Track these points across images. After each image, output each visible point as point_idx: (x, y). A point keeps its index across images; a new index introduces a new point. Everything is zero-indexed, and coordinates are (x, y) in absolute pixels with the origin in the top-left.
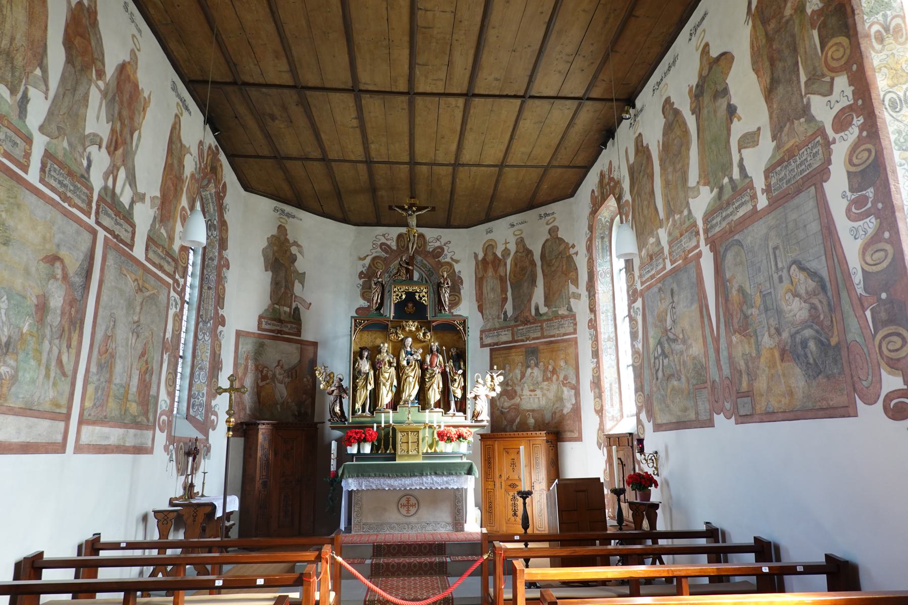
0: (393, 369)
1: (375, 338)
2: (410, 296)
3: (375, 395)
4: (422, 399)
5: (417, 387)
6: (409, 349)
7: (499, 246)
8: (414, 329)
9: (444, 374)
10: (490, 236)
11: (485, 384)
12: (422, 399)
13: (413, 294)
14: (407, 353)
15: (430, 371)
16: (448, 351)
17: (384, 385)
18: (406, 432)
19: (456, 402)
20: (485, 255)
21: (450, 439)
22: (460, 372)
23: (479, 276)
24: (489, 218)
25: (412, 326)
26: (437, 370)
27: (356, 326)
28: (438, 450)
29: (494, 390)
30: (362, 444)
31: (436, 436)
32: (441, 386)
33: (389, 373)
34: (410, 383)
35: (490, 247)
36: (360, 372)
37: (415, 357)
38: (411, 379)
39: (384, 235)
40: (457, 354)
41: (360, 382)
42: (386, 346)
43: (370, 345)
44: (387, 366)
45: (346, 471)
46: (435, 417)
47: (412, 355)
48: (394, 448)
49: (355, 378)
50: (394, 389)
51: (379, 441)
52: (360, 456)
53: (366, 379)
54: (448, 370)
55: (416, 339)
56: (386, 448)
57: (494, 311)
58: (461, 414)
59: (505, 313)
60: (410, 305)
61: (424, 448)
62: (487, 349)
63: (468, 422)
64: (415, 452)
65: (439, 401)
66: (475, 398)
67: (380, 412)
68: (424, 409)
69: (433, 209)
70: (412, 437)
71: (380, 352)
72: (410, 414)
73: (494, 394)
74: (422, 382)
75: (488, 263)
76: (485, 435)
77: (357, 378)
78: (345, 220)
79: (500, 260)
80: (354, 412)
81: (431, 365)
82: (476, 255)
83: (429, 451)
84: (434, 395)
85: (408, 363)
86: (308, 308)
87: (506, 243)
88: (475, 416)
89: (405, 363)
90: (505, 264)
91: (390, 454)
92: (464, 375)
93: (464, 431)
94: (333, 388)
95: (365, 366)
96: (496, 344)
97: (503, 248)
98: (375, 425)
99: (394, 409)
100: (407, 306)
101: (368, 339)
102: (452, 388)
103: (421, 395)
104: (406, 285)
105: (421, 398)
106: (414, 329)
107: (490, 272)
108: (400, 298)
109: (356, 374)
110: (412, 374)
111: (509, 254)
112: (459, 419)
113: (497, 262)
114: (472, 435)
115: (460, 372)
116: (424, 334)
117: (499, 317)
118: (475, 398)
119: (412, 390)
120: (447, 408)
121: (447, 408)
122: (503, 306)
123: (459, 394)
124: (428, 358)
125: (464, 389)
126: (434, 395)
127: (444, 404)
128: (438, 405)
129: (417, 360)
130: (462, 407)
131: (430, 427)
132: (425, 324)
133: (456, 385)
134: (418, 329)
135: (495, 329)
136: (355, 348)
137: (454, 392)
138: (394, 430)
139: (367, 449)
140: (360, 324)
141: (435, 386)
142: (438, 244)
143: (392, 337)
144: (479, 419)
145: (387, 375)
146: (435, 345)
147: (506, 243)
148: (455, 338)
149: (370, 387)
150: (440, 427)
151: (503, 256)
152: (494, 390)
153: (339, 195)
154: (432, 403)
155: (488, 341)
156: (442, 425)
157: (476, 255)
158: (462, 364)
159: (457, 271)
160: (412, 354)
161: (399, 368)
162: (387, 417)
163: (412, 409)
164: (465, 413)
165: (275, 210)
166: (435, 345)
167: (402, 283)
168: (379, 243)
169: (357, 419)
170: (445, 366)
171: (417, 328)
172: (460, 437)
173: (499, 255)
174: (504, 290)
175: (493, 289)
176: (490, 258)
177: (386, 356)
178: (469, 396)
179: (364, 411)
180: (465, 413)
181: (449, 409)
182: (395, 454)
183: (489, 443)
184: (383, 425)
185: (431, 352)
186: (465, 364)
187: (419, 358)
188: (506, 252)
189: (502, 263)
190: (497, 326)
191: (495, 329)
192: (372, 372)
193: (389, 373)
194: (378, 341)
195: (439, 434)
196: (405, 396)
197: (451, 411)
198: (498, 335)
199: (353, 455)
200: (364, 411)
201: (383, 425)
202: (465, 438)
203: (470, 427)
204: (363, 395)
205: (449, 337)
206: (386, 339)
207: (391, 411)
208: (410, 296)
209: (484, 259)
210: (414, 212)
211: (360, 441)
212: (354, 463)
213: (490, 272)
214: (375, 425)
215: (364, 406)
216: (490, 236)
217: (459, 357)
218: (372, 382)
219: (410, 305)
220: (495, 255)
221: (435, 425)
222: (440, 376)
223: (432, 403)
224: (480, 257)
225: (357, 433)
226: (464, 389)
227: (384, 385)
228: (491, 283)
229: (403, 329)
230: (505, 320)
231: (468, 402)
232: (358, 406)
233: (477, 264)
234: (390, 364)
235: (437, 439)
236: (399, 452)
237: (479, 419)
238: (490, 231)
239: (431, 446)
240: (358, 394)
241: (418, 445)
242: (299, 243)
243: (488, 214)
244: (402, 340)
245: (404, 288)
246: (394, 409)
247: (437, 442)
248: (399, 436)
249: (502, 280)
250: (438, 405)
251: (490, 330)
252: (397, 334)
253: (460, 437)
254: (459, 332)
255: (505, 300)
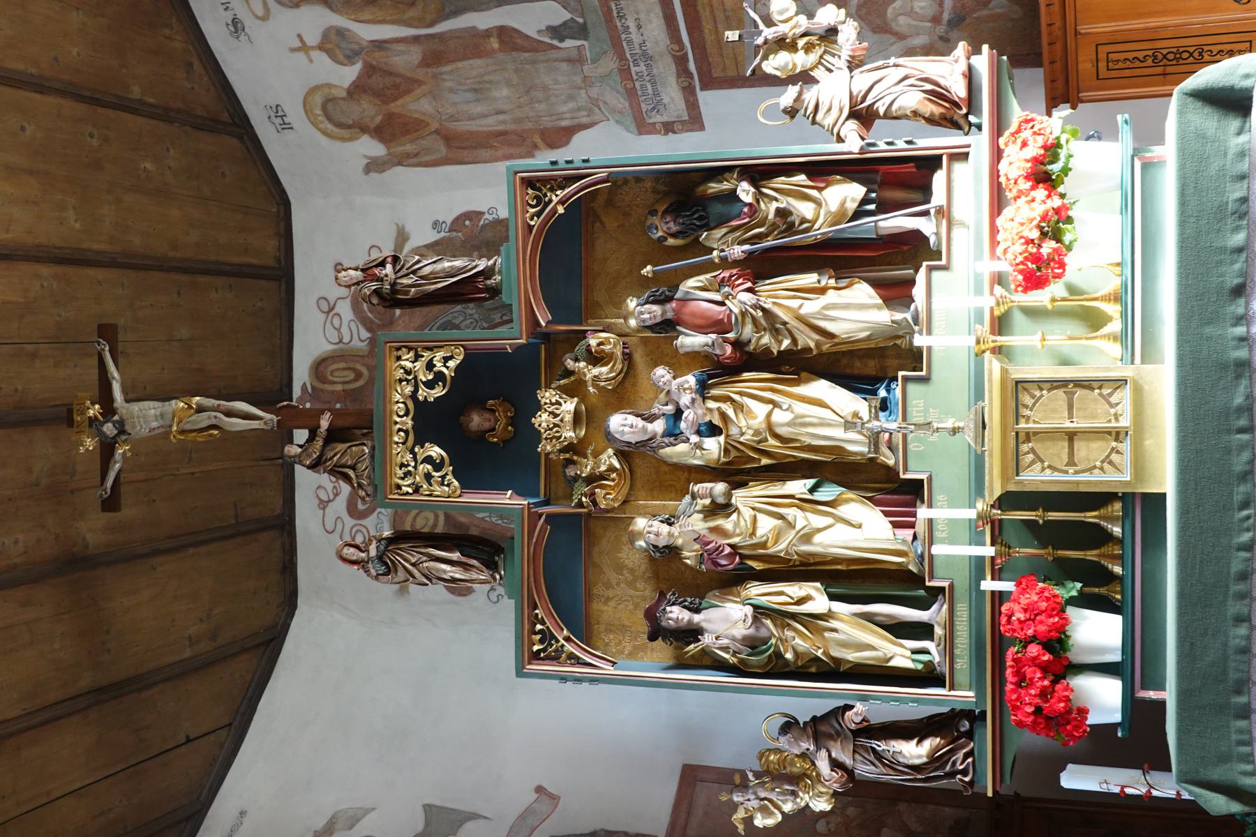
0: (740, 497)
1: (619, 568)
2: (431, 422)
3: (854, 579)
4: (871, 367)
5: (821, 388)
6: (659, 426)
7: (322, 79)
8: (569, 406)
9: (762, 266)
10: (295, 114)
11: (805, 78)
12: (871, 367)
13: (422, 411)
14: (673, 434)
15: (748, 331)
16: (660, 252)
17: (807, 538)
18: (1019, 441)
19: (886, 207)
20: (364, 130)
21: (1054, 226)
22: (745, 192)
23: (443, 150)
24: (231, 121)
25: (556, 413)
26: (743, 298)
27: (555, 658)
28: (1112, 284)
29: (832, 32)
30: (1075, 657)
31: (1039, 298)
32: (810, 279)
33: (757, 517)
34: (797, 422)
35: (333, 114)
36: (754, 644)
37: (685, 400)
38: (779, 417)
39: (323, 505)
40: (675, 210)
41: (797, 643)
42: (649, 528)
43: (647, 594)
44: (728, 524)
45: (1217, 774)
46: (952, 306)
47: (678, 414)
48: (1099, 499)
49: (778, 668)
50: (828, 492)
51: (1065, 571)
52: (1133, 667)
53: (782, 617)
54: (738, 251)
55: (622, 395)
56: (1099, 537)
57: (557, 79)
58: (939, 179)
59: (558, 32)
60: (477, 421)
61: (1101, 356)
62: (709, 100)
63: (979, 144)
64: (1124, 397)
65: (876, 284)
66: (863, 115)
67: (926, 559)
68: (915, 358)
69: (107, 332)
70: (1047, 414)
71: (671, 552)
72: (938, 423)
73: (849, 33)
74: (796, 365)
75: (390, 117)
76: (1050, 83)
77: (778, 655)
78: (267, 645)
79: (369, 70)
80: (928, 677)
81: (719, 326)
82: (374, 166)
83: (1115, 326)
84: (852, 310)
85: (713, 430)
86: (554, 798)
87: (304, 48)
88: (951, 113)
89: (713, 445)
90: (379, 45)
91: (1127, 515)
92: (760, 174)
93: (1016, 163)
94: (823, 765)
95: (726, 621)
96: (681, 61)
97: (321, 58)
98: (988, 585)
99: (914, 491)
100: (481, 435)
101: (621, 601)
102: (822, 229)
103: (858, 367)
104: (385, 444)
105: (871, 368)
106: (569, 406)
107: (419, 105)
108: (438, 466)
109: (762, 662)
110: (760, 410)
111: (341, 33)
112: (962, 188)
113: (377, 81)
114: (1037, 124)
115: (745, 192)
116: (596, 359)
117: (577, 60)
118: (863, 115)
119: (827, 412)
120: (912, 249)
121: (912, 249)
122: (532, 46)
123: (845, 194)
124: (691, 341)
125: (823, 171)
126: (852, 310)
127: (893, 262)
128: (896, 293)
129: (703, 389)
130: (906, 179)
131: (1001, 324)
132: (546, 357)
133: (805, 209)
134: (575, 388)
135: (625, 72)
136: (652, 663)
137: (839, 217)
138: (1008, 500)
139: (1096, 632)
140: (547, 637)
141: (810, 307)
142: (345, 309)
143: (607, 498)
144: (959, 89)
145: (766, 525)
146: (639, 311)
147: (304, 48)
148: (611, 222)
149: (819, 602)
150: (999, 279)
151: (350, 59)
152: (832, 32)
153: (107, 693)
154: (885, 316)
155: (672, 96)
156: (990, 267)
157: (374, 166)
158: (714, 187)
159: (433, 237)
160: (672, 410)
161: (738, 470)
162: (952, 532)
163: (916, 416)
164: (931, 163)
165: (886, 514)
166: (639, 311)
167: (380, 458)
168: (349, 522)
169: (963, 663)
170: (725, 263)
171: (569, 392)
172: (1043, 176)
173: (348, 74)
174: (474, 44)
175: (479, 91)
176: (368, 110)
177: (685, 527)
178: (852, 142)
179: (922, 631)
180: (931, 163)
181: (916, 238)
182: (1127, 499)
183: (1086, 66)
184: (988, 551)
185: (668, 326)
186: (717, 173)
187: (691, 380)
188: (335, 45)
189: (377, 58)
190: (610, 64)
191: (625, 72)
192: (756, 591)
193: (757, 517)
194: (632, 557)
195: (1033, 281)
196: (857, 445)
197: (926, 226)
198: (647, 57)
199: (1131, 703)
200: (922, 631)
201: (988, 551)
202: (1052, 150)
203: (999, 127)
204: (853, 631)
205: (608, 250)
206: (618, 520)
207: (923, 513)
208: (431, 422)
209: (379, 133)
210: (109, 409)
211: (1061, 662)
212: (1169, 695)
213: (419, 105)
214: (988, 585)
215: (900, 630)
216: (295, 114)
217: (690, 197)
218: (795, 590)
219: (477, 421)
220: (357, 89)
221: (987, 302)
222: (765, 287)
223: (885, 316)
224: (371, 147)
225: (1021, 678)
226: (823, 171)
227: (807, 538)
228: (457, 98)
229: (575, 449)
230: (581, 31)
231: (882, 148)
232: (901, 655)
233: (403, 160)
234: (720, 509)
235: (1056, 289)
236: (1117, 477)
237: (959, 89)
238: (278, 113)
239: (1094, 320)
240: (852, 656)
241: (1084, 384)
242: (320, 823)
243: (209, 125)
244: (620, 454)
245: (399, 453)
246: (914, 491)
247: (1073, 290)
248: (1036, 477)
249: (438, 53)
250: (896, 293)
251: (631, 94)
252: (594, 479)
253: (1043, 176)
254: (575, 207)
255: (506, 35)
